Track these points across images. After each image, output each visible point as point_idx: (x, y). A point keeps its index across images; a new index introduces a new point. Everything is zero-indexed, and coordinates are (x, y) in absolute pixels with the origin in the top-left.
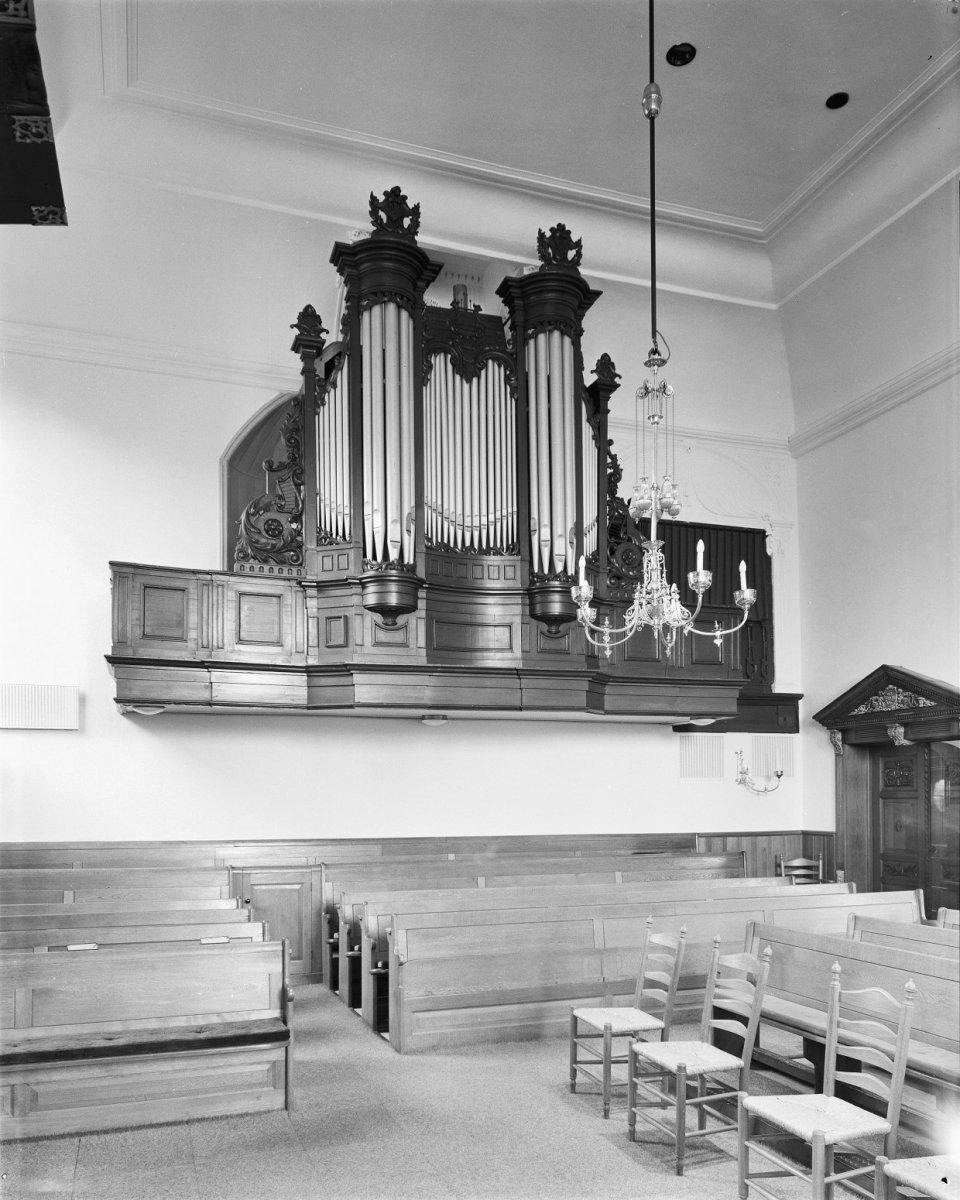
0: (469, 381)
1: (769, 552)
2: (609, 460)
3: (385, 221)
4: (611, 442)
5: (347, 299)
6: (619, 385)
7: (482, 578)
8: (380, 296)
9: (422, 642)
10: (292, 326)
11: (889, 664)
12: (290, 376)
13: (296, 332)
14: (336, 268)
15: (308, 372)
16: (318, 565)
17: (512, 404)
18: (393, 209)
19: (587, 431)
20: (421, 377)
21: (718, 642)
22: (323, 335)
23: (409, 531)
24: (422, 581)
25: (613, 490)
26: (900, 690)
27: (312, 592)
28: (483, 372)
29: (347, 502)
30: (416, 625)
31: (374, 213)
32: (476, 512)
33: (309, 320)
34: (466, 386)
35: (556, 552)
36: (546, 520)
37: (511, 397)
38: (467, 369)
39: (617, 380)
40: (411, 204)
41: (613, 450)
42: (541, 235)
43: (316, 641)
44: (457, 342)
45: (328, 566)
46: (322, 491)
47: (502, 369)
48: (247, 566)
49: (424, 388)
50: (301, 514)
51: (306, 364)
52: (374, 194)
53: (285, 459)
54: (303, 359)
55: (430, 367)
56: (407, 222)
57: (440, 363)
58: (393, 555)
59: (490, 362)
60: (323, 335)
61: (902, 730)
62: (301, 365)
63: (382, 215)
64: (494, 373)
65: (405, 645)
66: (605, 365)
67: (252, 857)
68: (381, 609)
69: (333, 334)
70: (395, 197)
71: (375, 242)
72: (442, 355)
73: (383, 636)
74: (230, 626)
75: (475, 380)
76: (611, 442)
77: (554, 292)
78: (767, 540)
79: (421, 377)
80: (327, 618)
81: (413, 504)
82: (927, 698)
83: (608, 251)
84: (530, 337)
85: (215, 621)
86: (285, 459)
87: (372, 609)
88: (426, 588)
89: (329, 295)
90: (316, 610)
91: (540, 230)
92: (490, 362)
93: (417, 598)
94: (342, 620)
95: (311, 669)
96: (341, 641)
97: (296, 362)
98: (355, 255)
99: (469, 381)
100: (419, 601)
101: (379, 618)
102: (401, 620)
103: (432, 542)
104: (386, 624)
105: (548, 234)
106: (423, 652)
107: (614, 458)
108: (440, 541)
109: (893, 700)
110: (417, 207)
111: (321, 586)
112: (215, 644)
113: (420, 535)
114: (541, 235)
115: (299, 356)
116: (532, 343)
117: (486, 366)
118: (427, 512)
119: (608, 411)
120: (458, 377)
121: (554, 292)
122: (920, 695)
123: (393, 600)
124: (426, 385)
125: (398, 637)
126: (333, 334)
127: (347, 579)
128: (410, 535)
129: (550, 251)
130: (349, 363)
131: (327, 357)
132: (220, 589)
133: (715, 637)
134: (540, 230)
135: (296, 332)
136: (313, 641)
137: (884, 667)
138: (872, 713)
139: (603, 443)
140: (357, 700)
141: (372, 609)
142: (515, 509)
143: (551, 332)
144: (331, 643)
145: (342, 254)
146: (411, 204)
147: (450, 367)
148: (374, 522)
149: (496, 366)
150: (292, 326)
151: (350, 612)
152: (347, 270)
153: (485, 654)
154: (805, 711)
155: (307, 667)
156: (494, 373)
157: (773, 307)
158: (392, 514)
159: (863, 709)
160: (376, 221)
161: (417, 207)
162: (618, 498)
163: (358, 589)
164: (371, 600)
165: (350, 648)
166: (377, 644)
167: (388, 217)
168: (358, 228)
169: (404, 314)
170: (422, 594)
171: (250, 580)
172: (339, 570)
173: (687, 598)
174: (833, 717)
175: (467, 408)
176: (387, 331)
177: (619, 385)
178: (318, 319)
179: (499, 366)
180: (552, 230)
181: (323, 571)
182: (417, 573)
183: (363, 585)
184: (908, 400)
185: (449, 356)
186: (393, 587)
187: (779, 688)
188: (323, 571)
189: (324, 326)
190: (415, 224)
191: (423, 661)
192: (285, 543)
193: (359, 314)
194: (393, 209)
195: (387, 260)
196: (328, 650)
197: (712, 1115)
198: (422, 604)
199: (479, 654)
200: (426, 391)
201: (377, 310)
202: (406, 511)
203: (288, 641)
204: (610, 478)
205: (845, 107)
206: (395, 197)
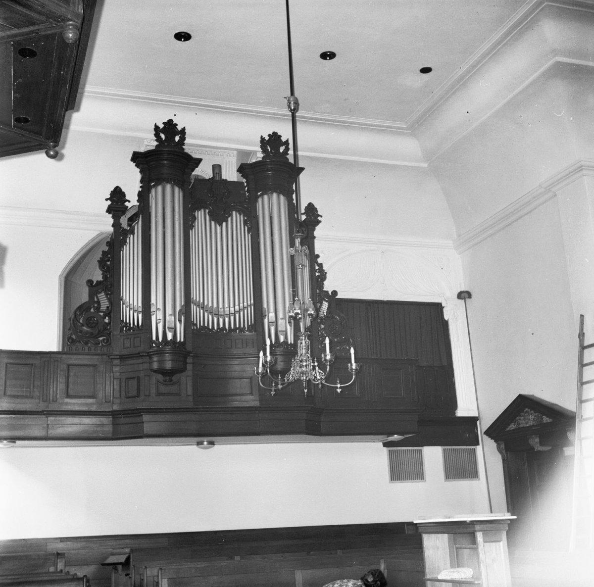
0: (221, 225)
1: (446, 318)
2: (317, 268)
3: (164, 139)
4: (318, 256)
5: (141, 181)
6: (320, 222)
7: (232, 348)
8: (160, 181)
9: (190, 392)
10: (107, 200)
11: (523, 393)
12: (106, 225)
13: (109, 202)
14: (135, 164)
15: (116, 225)
16: (120, 346)
17: (248, 238)
18: (169, 132)
19: (118, 357)
20: (188, 224)
21: (339, 391)
22: (127, 204)
23: (180, 321)
24: (189, 352)
25: (321, 286)
26: (532, 412)
27: (117, 362)
28: (229, 219)
29: (140, 304)
30: (186, 381)
31: (157, 135)
32: (226, 305)
33: (117, 195)
34: (218, 228)
35: (280, 329)
36: (272, 309)
37: (248, 233)
38: (219, 217)
39: (319, 218)
40: (179, 128)
41: (320, 261)
42: (262, 139)
43: (119, 394)
44: (213, 199)
45: (127, 345)
46: (124, 298)
47: (242, 216)
48: (74, 348)
49: (191, 231)
50: (110, 312)
51: (114, 220)
52: (157, 125)
53: (100, 278)
54: (113, 217)
55: (194, 219)
56: (177, 138)
57: (200, 215)
58: (170, 336)
59: (234, 212)
60: (127, 204)
61: (537, 440)
62: (111, 221)
63: (163, 136)
64: (237, 219)
65: (178, 394)
66: (311, 208)
67: (73, 550)
68: (162, 371)
69: (132, 200)
70: (170, 126)
71: (157, 151)
72: (202, 210)
73: (163, 389)
74: (61, 386)
75: (224, 224)
76: (318, 256)
77: (275, 168)
78: (444, 310)
79: (188, 224)
80: (127, 379)
81: (183, 303)
82: (547, 417)
83: (311, 141)
84: (259, 197)
85: (52, 384)
86: (100, 278)
87: (156, 371)
88: (192, 356)
89: (131, 182)
90: (118, 374)
91: (262, 136)
92: (234, 212)
93: (185, 363)
94: (136, 379)
95: (115, 413)
96: (135, 393)
97: (109, 219)
98: (146, 157)
99: (221, 225)
100: (188, 365)
101: (160, 377)
102: (174, 378)
103: (197, 326)
104: (165, 381)
105: (267, 138)
106: (191, 398)
107: (321, 265)
108: (202, 325)
109: (529, 419)
110: (184, 129)
111: (122, 358)
112: (51, 399)
113: (189, 323)
114: (262, 139)
115: (111, 215)
116: (260, 200)
117: (231, 215)
118: (193, 307)
119: (315, 237)
120: (213, 223)
121: (275, 168)
122: (544, 414)
123: (168, 365)
124: (192, 229)
125: (173, 389)
126: (132, 200)
127: (139, 353)
128: (181, 323)
129: (269, 148)
130: (142, 217)
131: (129, 214)
132: (56, 363)
133: (337, 388)
134: (262, 136)
135: (109, 202)
136: (117, 394)
137: (520, 396)
138: (519, 428)
139: (313, 258)
140: (145, 432)
141: (156, 371)
142: (252, 301)
143: (272, 193)
144: (130, 395)
145: (138, 157)
146: (179, 128)
147: (208, 217)
148: (156, 317)
149: (238, 215)
150: (107, 200)
151: (142, 375)
152: (141, 166)
153: (234, 398)
154: (484, 425)
155: (112, 412)
156: (237, 219)
157: (426, 165)
158: (169, 311)
159: (512, 427)
160: (158, 138)
161: (184, 129)
162: (325, 291)
163: (147, 359)
164: (155, 366)
165: (142, 397)
166: (159, 394)
167: (165, 136)
168: (149, 143)
169: (177, 190)
170: (189, 360)
171: (76, 357)
172: (134, 347)
173: (322, 366)
174: (496, 431)
175: (219, 245)
176: (167, 200)
177: (320, 222)
178: (123, 195)
179: (240, 215)
180: (269, 135)
181: (124, 348)
182: (187, 348)
183: (150, 356)
184: (518, 220)
185: (207, 211)
186: (168, 357)
187: (460, 413)
188: (124, 348)
189: (127, 198)
190: (183, 139)
191: (190, 405)
192: (99, 331)
193: (149, 191)
194: (169, 132)
196: (128, 400)
197: (146, 574)
198: (189, 367)
199: (230, 398)
200: (192, 233)
201: (160, 188)
202: (178, 308)
203: (101, 395)
204: (318, 277)
205: (430, 73)
206: (170, 126)
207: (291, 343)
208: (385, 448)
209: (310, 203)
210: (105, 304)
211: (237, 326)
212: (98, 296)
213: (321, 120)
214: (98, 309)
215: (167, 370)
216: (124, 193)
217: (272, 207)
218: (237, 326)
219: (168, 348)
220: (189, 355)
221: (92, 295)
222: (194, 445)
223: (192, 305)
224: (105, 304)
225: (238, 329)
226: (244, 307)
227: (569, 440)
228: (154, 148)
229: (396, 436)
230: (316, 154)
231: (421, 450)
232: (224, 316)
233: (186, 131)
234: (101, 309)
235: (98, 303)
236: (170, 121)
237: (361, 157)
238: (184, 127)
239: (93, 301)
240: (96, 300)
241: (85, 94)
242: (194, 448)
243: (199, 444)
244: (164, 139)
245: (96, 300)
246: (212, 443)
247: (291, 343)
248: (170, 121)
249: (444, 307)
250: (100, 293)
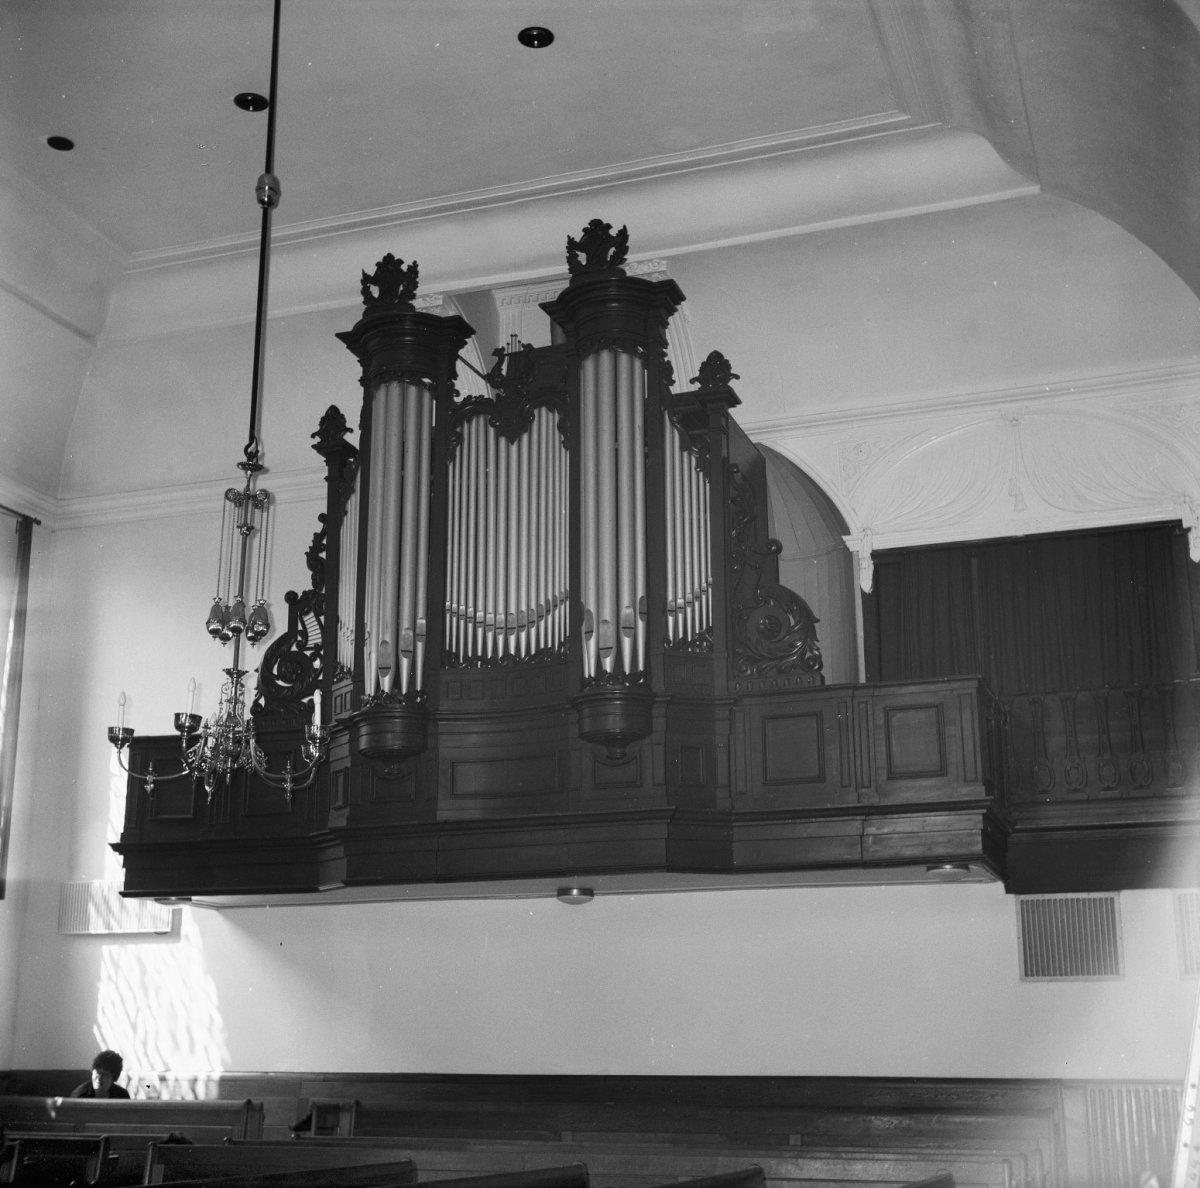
5: (665, 344)
69: (353, 420)
70: (389, 264)
77: (611, 299)
78: (1191, 536)
121: (611, 299)
175: (515, 488)
178: (726, 365)
195: (398, 332)
206: (389, 264)
207: (590, 676)
208: (1012, 897)
209: (716, 352)
210: (315, 637)
211: (480, 654)
212: (305, 619)
213: (795, 148)
214: (302, 646)
215: (392, 752)
216: (727, 361)
217: (609, 384)
218: (480, 654)
219: (398, 709)
220: (655, 702)
221: (294, 617)
222: (551, 896)
223: (448, 616)
224: (315, 637)
225: (479, 659)
226: (701, 591)
227: (994, 881)
228: (566, 285)
229: (948, 867)
230: (782, 230)
231: (1112, 900)
232: (496, 629)
233: (419, 268)
234: (310, 643)
235: (305, 633)
236: (389, 257)
237: (646, 251)
238: (625, 227)
239: (294, 632)
240: (300, 628)
241: (272, 245)
242: (553, 903)
243: (563, 892)
244: (584, 263)
245: (300, 628)
246: (588, 892)
247: (590, 676)
248: (389, 257)
249: (1189, 529)
250: (307, 613)
